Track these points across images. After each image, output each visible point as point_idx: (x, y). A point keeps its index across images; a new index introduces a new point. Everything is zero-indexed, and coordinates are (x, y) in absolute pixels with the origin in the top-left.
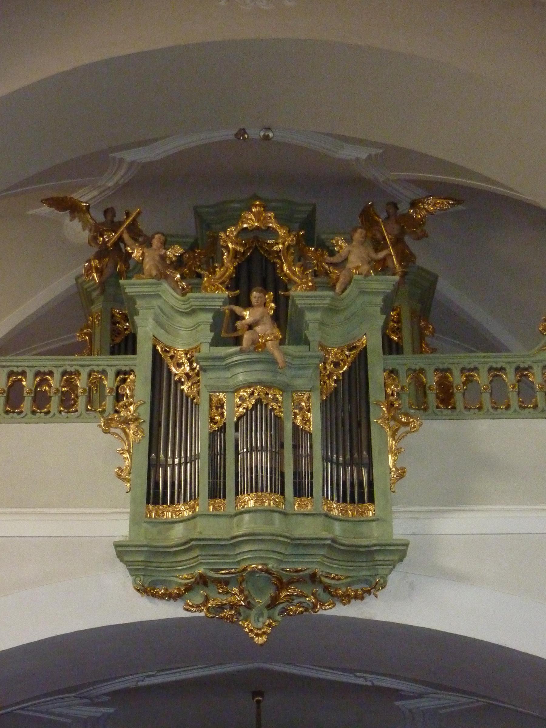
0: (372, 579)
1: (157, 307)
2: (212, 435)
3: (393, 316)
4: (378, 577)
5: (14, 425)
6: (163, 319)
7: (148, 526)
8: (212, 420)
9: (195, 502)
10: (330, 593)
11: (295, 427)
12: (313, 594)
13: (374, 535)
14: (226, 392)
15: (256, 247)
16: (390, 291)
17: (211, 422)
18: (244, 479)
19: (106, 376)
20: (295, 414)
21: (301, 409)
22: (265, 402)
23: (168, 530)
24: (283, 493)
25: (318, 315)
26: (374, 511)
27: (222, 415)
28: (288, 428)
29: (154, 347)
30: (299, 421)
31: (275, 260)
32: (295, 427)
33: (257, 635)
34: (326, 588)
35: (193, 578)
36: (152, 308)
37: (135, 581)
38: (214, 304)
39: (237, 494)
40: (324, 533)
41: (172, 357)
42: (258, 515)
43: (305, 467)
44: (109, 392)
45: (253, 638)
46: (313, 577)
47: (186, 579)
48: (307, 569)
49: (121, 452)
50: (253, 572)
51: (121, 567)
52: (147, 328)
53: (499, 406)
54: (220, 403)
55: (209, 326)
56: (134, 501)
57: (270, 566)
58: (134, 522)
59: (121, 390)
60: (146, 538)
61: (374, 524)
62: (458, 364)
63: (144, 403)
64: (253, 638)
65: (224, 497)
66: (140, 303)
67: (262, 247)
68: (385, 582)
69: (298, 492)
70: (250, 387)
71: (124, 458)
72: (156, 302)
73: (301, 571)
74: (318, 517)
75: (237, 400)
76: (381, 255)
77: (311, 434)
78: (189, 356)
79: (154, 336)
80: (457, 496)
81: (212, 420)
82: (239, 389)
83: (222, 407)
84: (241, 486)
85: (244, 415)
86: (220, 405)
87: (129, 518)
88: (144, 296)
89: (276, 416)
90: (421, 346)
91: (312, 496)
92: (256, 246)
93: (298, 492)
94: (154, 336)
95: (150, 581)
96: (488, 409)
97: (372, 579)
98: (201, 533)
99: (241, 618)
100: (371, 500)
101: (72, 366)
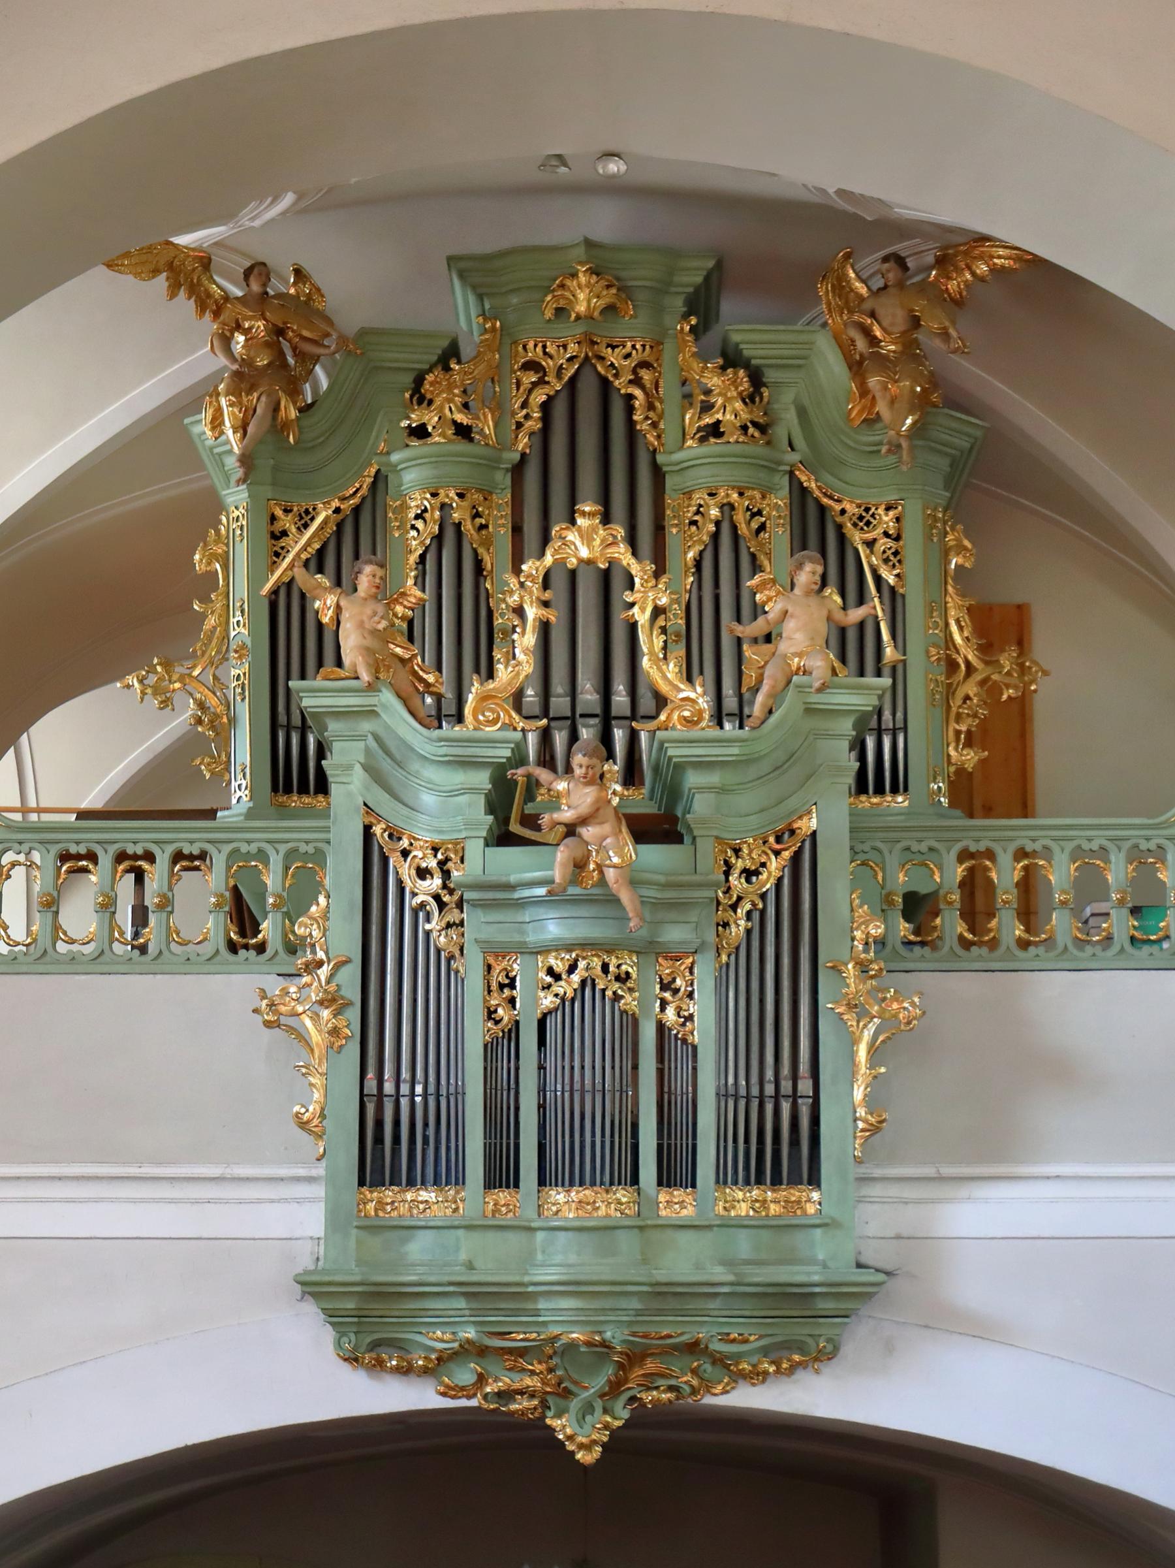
0: (810, 1341)
1: (370, 737)
2: (490, 1049)
3: (887, 523)
4: (822, 1339)
5: (77, 977)
6: (386, 764)
7: (362, 1233)
8: (491, 1013)
9: (457, 1192)
10: (727, 1367)
11: (661, 1027)
12: (694, 1372)
13: (820, 1260)
14: (521, 953)
15: (587, 357)
16: (870, 708)
17: (490, 1018)
18: (558, 1147)
19: (266, 863)
20: (664, 1004)
21: (676, 991)
22: (600, 985)
23: (404, 1241)
24: (635, 1180)
25: (714, 778)
26: (820, 1204)
27: (512, 1001)
28: (648, 1034)
29: (367, 829)
30: (670, 1014)
31: (630, 391)
32: (661, 1027)
33: (581, 1446)
34: (719, 1360)
35: (454, 1341)
36: (362, 738)
37: (338, 1345)
38: (490, 752)
39: (542, 1182)
40: (719, 1269)
41: (405, 853)
42: (585, 1236)
43: (679, 1082)
44: (274, 905)
45: (573, 1453)
46: (694, 1348)
47: (443, 1341)
48: (682, 1334)
49: (304, 1070)
50: (572, 1346)
51: (311, 1309)
52: (351, 787)
53: (1091, 948)
54: (507, 976)
55: (483, 796)
56: (331, 1180)
57: (608, 1335)
58: (335, 1221)
59: (299, 927)
60: (360, 1262)
61: (818, 1231)
62: (1011, 840)
63: (348, 961)
64: (573, 1453)
65: (517, 1186)
66: (334, 727)
67: (602, 359)
68: (836, 1349)
69: (665, 1180)
70: (570, 951)
71: (311, 1085)
72: (366, 726)
73: (669, 1336)
74: (708, 1229)
75: (542, 975)
76: (856, 614)
77: (695, 1048)
78: (440, 856)
79: (365, 804)
80: (990, 1147)
81: (491, 1013)
82: (548, 951)
83: (512, 986)
84: (550, 1166)
85: (556, 1009)
86: (507, 981)
87: (323, 1194)
88: (339, 715)
89: (623, 1012)
90: (946, 590)
91: (694, 1186)
92: (587, 355)
93: (665, 1180)
94: (365, 804)
95: (368, 1340)
96: (1066, 947)
97: (810, 1341)
98: (470, 1266)
99: (550, 1414)
100: (814, 1180)
101: (191, 842)
